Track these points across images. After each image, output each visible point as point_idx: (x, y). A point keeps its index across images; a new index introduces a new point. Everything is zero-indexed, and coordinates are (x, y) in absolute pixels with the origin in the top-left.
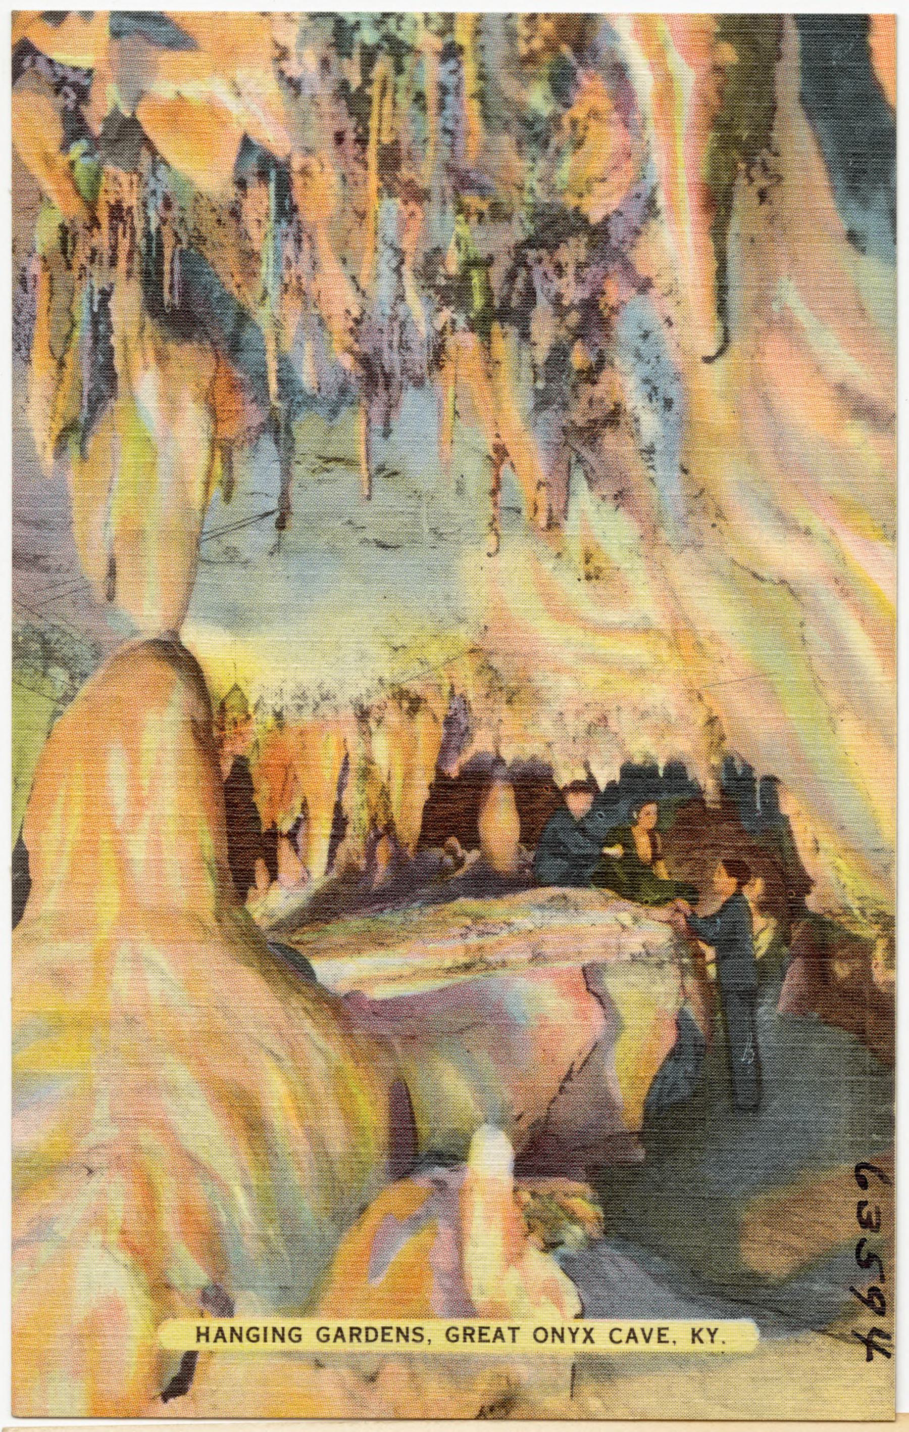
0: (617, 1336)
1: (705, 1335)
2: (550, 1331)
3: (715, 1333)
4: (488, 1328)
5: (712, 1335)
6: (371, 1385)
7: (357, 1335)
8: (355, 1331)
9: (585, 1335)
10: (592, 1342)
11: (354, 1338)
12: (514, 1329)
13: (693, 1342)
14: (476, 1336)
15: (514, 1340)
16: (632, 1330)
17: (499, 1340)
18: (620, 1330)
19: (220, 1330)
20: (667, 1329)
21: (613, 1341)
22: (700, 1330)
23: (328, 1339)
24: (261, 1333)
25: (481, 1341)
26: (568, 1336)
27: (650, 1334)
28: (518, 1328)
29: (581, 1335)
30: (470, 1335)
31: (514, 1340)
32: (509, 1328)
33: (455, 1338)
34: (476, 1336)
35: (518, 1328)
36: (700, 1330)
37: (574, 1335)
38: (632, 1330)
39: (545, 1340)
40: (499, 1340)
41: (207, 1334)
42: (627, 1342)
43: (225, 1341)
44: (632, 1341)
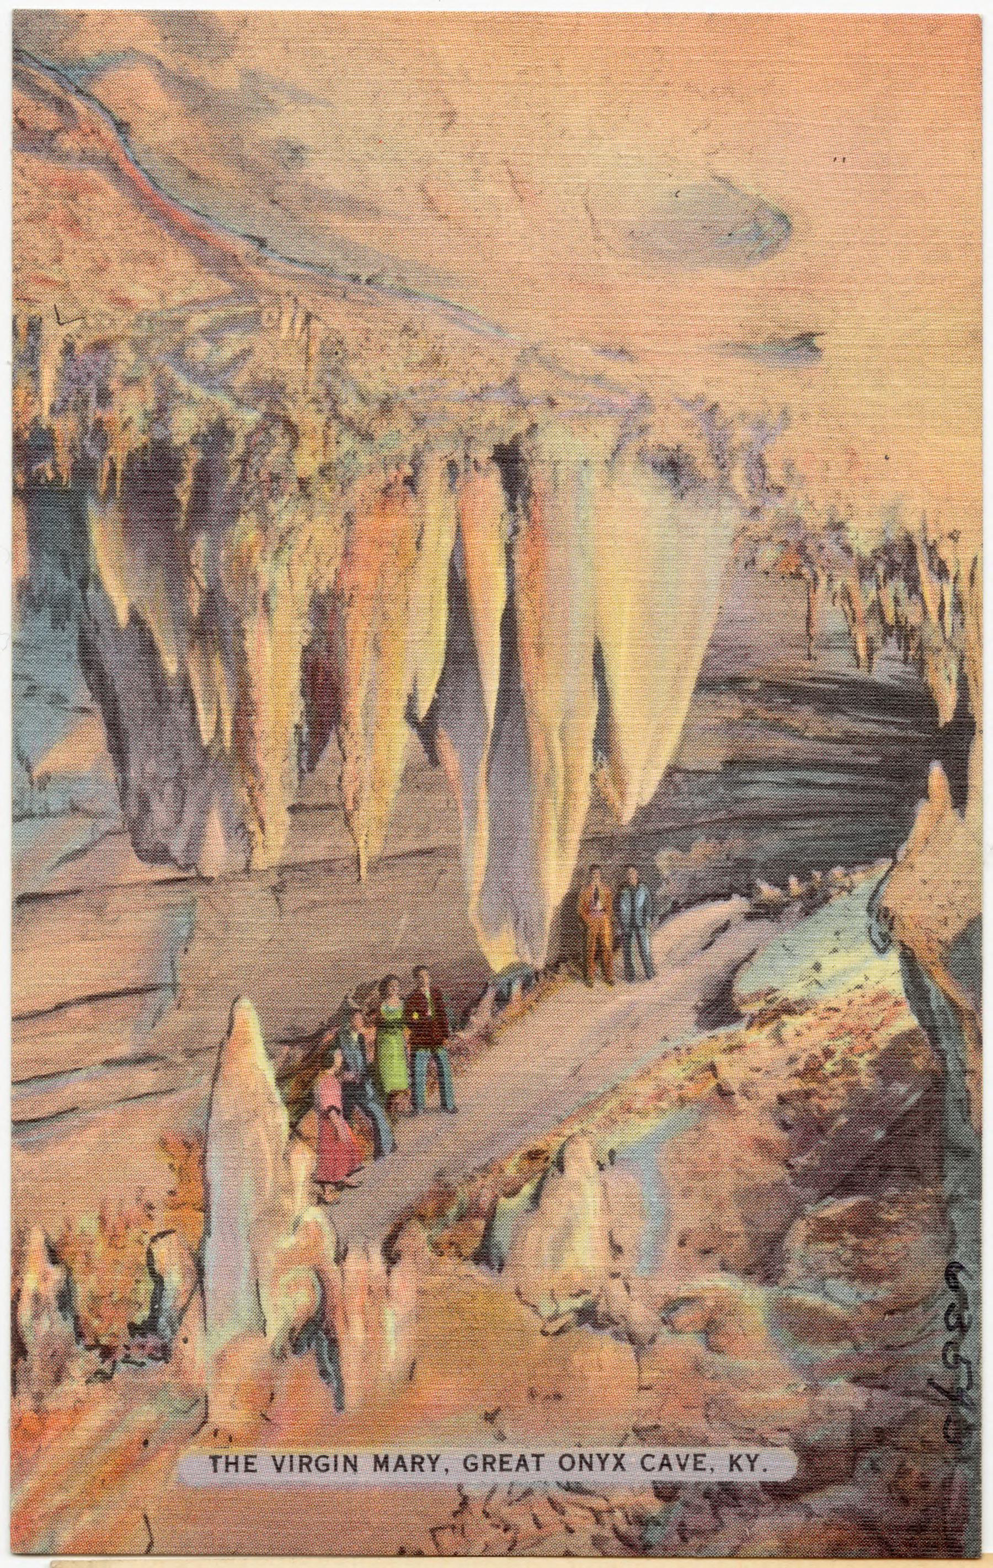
0: (649, 1462)
1: (744, 1462)
2: (577, 1460)
3: (437, 1459)
4: (510, 1456)
5: (433, 1463)
6: (796, 221)
7: (307, 1465)
8: (305, 1460)
9: (615, 1461)
10: (623, 1469)
11: (417, 1467)
12: (538, 1456)
13: (731, 1470)
14: (497, 1465)
15: (538, 1469)
16: (666, 1457)
17: (522, 1469)
18: (653, 1456)
19: (401, 1458)
20: (255, 1457)
21: (647, 1470)
22: (739, 1457)
23: (476, 1468)
24: (331, 1461)
25: (502, 1469)
26: (427, 1464)
27: (345, 1466)
28: (543, 1455)
29: (611, 1461)
30: (307, 1465)
31: (538, 1469)
32: (533, 1455)
33: (473, 1467)
34: (497, 1465)
35: (543, 1455)
36: (739, 1457)
37: (603, 1462)
38: (666, 1457)
39: (572, 1467)
40: (522, 1469)
41: (228, 1464)
42: (660, 1469)
43: (406, 1470)
44: (665, 1469)
